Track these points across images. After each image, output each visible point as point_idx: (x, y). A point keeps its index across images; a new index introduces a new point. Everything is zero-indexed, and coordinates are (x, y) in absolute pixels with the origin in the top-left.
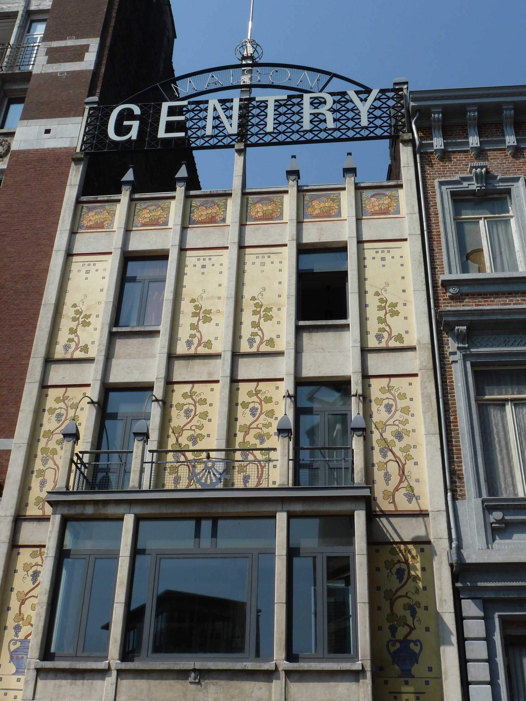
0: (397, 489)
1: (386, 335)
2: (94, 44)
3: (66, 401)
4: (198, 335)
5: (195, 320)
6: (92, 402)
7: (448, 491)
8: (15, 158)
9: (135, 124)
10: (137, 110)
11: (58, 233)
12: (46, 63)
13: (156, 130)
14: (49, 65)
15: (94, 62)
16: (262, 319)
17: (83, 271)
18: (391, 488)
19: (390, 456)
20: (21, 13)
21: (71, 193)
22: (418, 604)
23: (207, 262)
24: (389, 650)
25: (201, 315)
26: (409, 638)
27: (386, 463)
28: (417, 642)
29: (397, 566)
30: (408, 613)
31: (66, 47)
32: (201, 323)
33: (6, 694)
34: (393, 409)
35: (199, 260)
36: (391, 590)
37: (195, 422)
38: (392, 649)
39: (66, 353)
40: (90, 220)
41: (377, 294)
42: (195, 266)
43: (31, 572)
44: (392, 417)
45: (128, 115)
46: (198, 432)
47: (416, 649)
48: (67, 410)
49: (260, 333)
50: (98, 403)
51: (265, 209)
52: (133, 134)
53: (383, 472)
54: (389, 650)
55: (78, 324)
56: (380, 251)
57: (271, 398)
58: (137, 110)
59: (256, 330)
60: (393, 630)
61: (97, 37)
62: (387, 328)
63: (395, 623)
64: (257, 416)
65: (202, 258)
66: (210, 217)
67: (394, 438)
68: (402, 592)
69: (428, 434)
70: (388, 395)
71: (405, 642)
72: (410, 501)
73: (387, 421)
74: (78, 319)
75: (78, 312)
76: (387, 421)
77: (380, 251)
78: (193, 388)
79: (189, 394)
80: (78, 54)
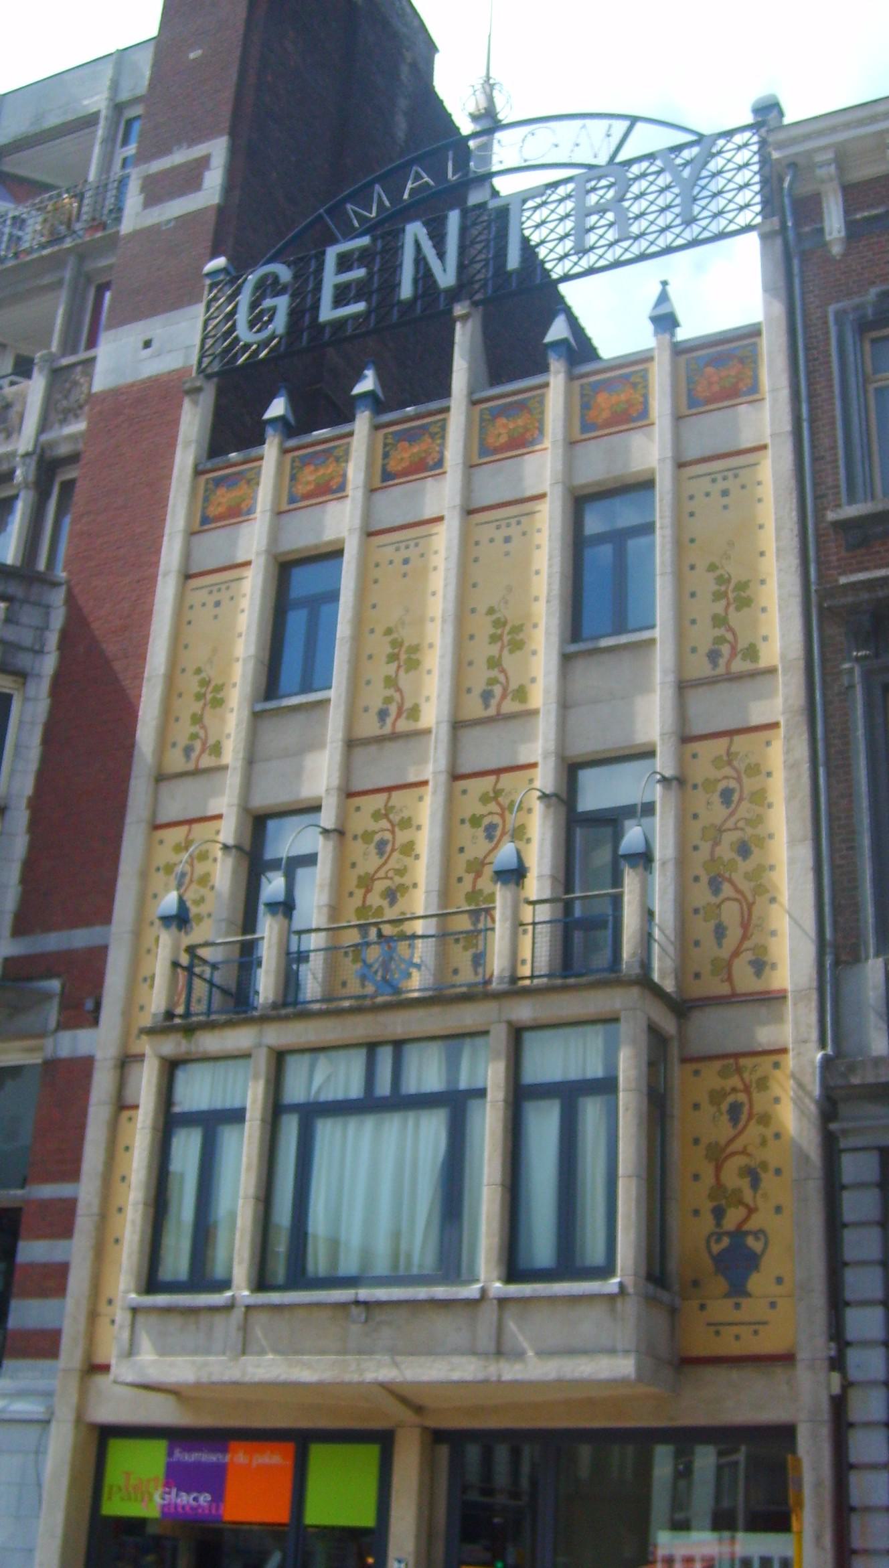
0: (736, 954)
2: (217, 150)
3: (735, 763)
4: (397, 696)
5: (719, 608)
6: (226, 847)
7: (828, 950)
8: (98, 408)
9: (282, 303)
10: (284, 273)
11: (166, 539)
13: (316, 307)
15: (218, 188)
16: (732, 608)
17: (210, 605)
18: (725, 953)
19: (727, 890)
20: (103, 113)
21: (185, 458)
22: (764, 1165)
23: (412, 553)
24: (710, 1252)
25: (403, 657)
26: (746, 1227)
27: (719, 906)
28: (759, 1233)
29: (731, 1099)
30: (744, 1184)
31: (174, 169)
32: (506, 652)
33: (756, 1332)
34: (736, 797)
35: (397, 549)
36: (717, 1144)
37: (392, 863)
38: (716, 1248)
39: (381, 727)
40: (219, 504)
41: (712, 568)
44: (732, 814)
45: (269, 286)
46: (398, 880)
48: (393, 832)
49: (502, 678)
50: (238, 847)
51: (511, 426)
52: (279, 324)
53: (711, 925)
54: (710, 1252)
55: (728, 605)
56: (719, 477)
57: (410, 819)
58: (284, 273)
59: (495, 673)
60: (719, 1213)
61: (222, 135)
62: (729, 636)
63: (723, 1202)
64: (496, 840)
67: (733, 855)
68: (737, 1145)
69: (792, 842)
70: (727, 771)
71: (739, 1234)
73: (376, 872)
74: (204, 695)
75: (205, 683)
76: (376, 872)
77: (719, 477)
78: (190, 831)
79: (725, 758)
80: (190, 178)
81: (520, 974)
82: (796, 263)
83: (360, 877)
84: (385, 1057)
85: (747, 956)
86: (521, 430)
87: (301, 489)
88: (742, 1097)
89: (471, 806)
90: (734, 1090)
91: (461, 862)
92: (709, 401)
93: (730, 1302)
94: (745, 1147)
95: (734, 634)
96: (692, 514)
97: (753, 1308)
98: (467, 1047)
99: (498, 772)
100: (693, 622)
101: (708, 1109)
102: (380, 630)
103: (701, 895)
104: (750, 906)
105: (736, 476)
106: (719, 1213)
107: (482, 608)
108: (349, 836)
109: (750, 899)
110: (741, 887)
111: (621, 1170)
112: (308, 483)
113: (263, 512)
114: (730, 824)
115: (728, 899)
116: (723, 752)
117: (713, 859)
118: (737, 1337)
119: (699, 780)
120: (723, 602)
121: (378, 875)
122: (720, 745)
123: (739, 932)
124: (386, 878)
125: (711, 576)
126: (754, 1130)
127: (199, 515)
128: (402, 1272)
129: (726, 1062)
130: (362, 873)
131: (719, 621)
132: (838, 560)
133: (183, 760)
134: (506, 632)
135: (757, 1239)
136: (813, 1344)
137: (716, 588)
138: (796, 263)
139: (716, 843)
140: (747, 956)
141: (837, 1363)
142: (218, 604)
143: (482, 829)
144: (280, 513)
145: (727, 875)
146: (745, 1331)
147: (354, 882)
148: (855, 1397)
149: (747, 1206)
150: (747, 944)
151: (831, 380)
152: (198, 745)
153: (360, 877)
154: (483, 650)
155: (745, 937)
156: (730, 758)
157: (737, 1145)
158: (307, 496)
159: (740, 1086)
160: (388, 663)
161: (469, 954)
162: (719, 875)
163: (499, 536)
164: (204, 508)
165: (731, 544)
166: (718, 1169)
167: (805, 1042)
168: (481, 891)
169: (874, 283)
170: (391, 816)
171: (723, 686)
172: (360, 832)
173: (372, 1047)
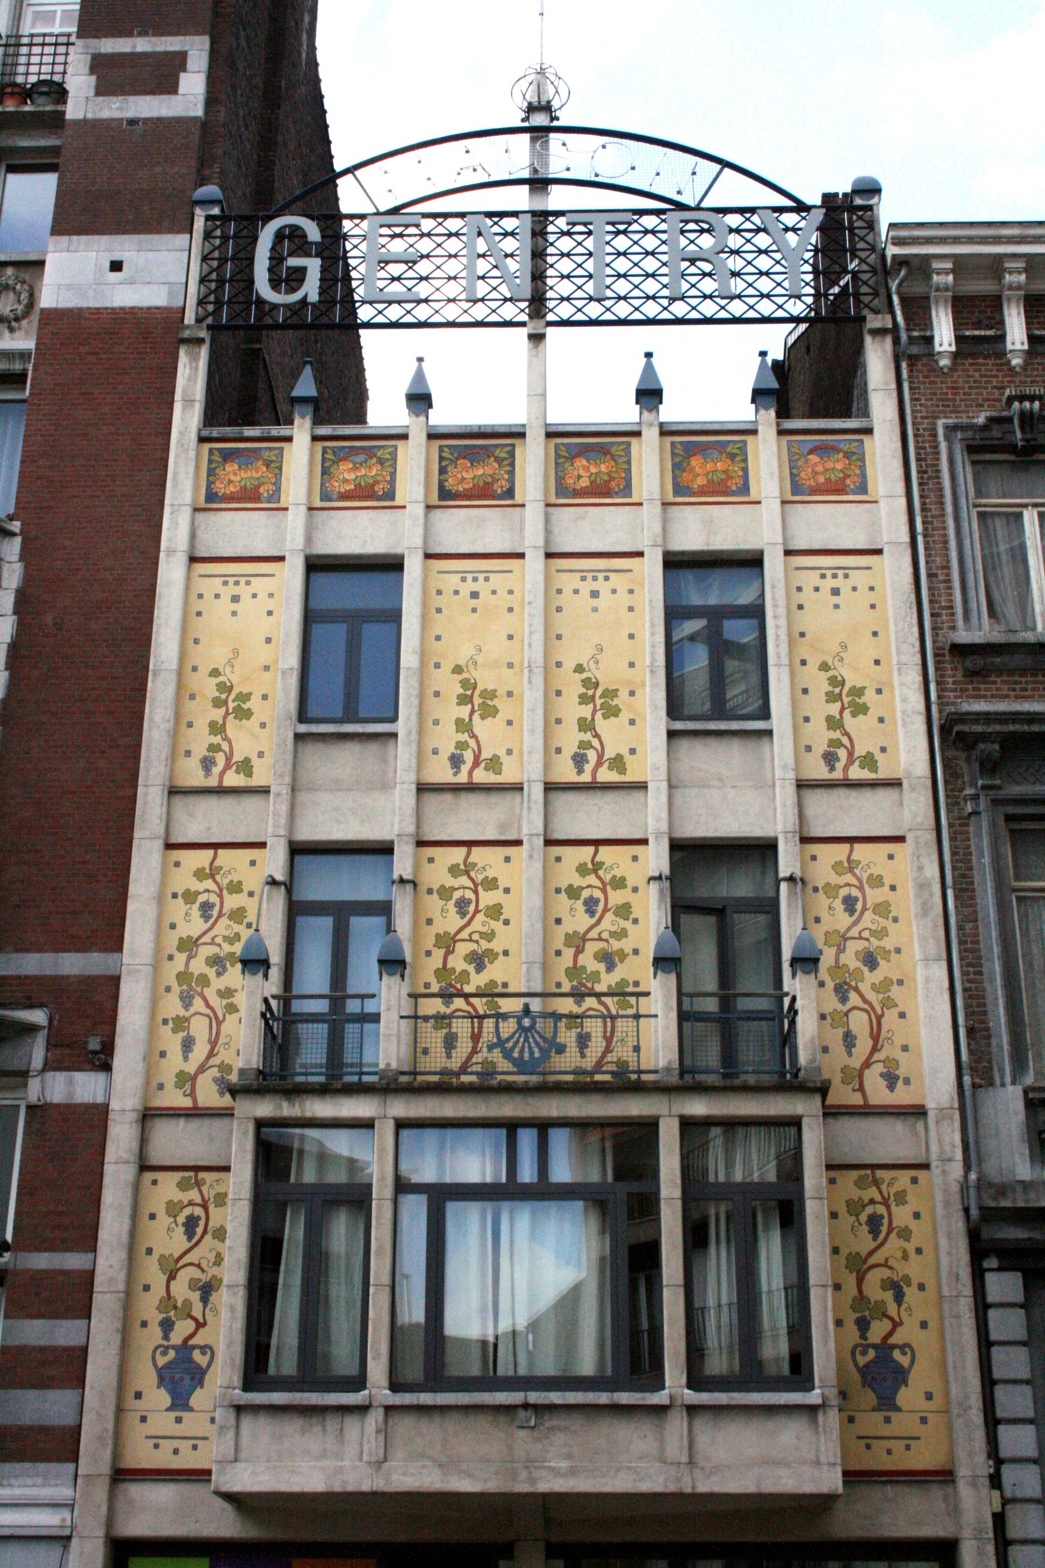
0: (867, 1064)
1: (842, 754)
2: (197, 51)
12: (92, 93)
14: (101, 98)
17: (226, 598)
19: (854, 999)
22: (907, 1280)
25: (477, 700)
26: (892, 1340)
27: (846, 1014)
28: (904, 1348)
29: (869, 1210)
30: (888, 1296)
33: (908, 1447)
37: (477, 924)
38: (862, 1361)
39: (455, 774)
40: (230, 482)
41: (824, 667)
42: (456, 592)
43: (181, 1219)
46: (484, 945)
47: (904, 1361)
51: (593, 470)
53: (840, 1032)
60: (167, 1326)
62: (845, 740)
63: (867, 1313)
64: (597, 915)
65: (470, 577)
66: (481, 484)
67: (859, 964)
68: (878, 1258)
71: (884, 1348)
72: (891, 1087)
77: (829, 573)
79: (846, 865)
80: (163, 75)
81: (701, 1063)
82: (904, 365)
83: (438, 935)
84: (527, 1139)
85: (879, 1068)
86: (606, 478)
87: (337, 487)
88: (881, 1209)
89: (567, 875)
90: (872, 1201)
91: (172, 939)
92: (814, 491)
93: (879, 1416)
94: (887, 1260)
95: (478, 742)
96: (439, 611)
97: (903, 1423)
98: (741, 1131)
99: (597, 843)
100: (436, 722)
101: (164, 1219)
102: (447, 667)
103: (172, 1006)
104: (879, 1018)
105: (846, 576)
106: (167, 1326)
107: (569, 665)
108: (423, 888)
109: (221, 1018)
110: (212, 1002)
111: (813, 1279)
112: (346, 481)
113: (176, 508)
114: (854, 932)
115: (854, 1008)
116: (844, 858)
117: (837, 965)
118: (889, 1452)
119: (820, 885)
120: (838, 705)
121: (849, 935)
122: (458, 855)
123: (870, 1043)
124: (600, 939)
125: (824, 676)
126: (894, 1244)
127: (203, 491)
128: (522, 1371)
129: (862, 1172)
130: (184, 936)
131: (834, 723)
132: (954, 683)
133: (201, 773)
134: (844, 692)
135: (204, 1353)
136: (972, 1461)
137: (461, 691)
138: (904, 365)
139: (841, 950)
140: (879, 1068)
141: (995, 1481)
142: (235, 599)
143: (581, 901)
144: (310, 509)
145: (853, 984)
146: (898, 1446)
147: (432, 940)
148: (1013, 1514)
149: (890, 1318)
150: (877, 1056)
151: (942, 496)
152: (221, 759)
153: (438, 935)
154: (572, 710)
155: (875, 1049)
156: (851, 866)
157: (878, 1258)
158: (343, 497)
159: (878, 1198)
160: (458, 704)
161: (573, 1033)
162: (845, 983)
163: (227, 593)
164: (210, 484)
165: (844, 647)
166: (860, 1281)
167: (949, 1160)
168: (584, 968)
169: (982, 406)
170: (218, 878)
171: (843, 792)
172: (564, 885)
173: (512, 1127)
